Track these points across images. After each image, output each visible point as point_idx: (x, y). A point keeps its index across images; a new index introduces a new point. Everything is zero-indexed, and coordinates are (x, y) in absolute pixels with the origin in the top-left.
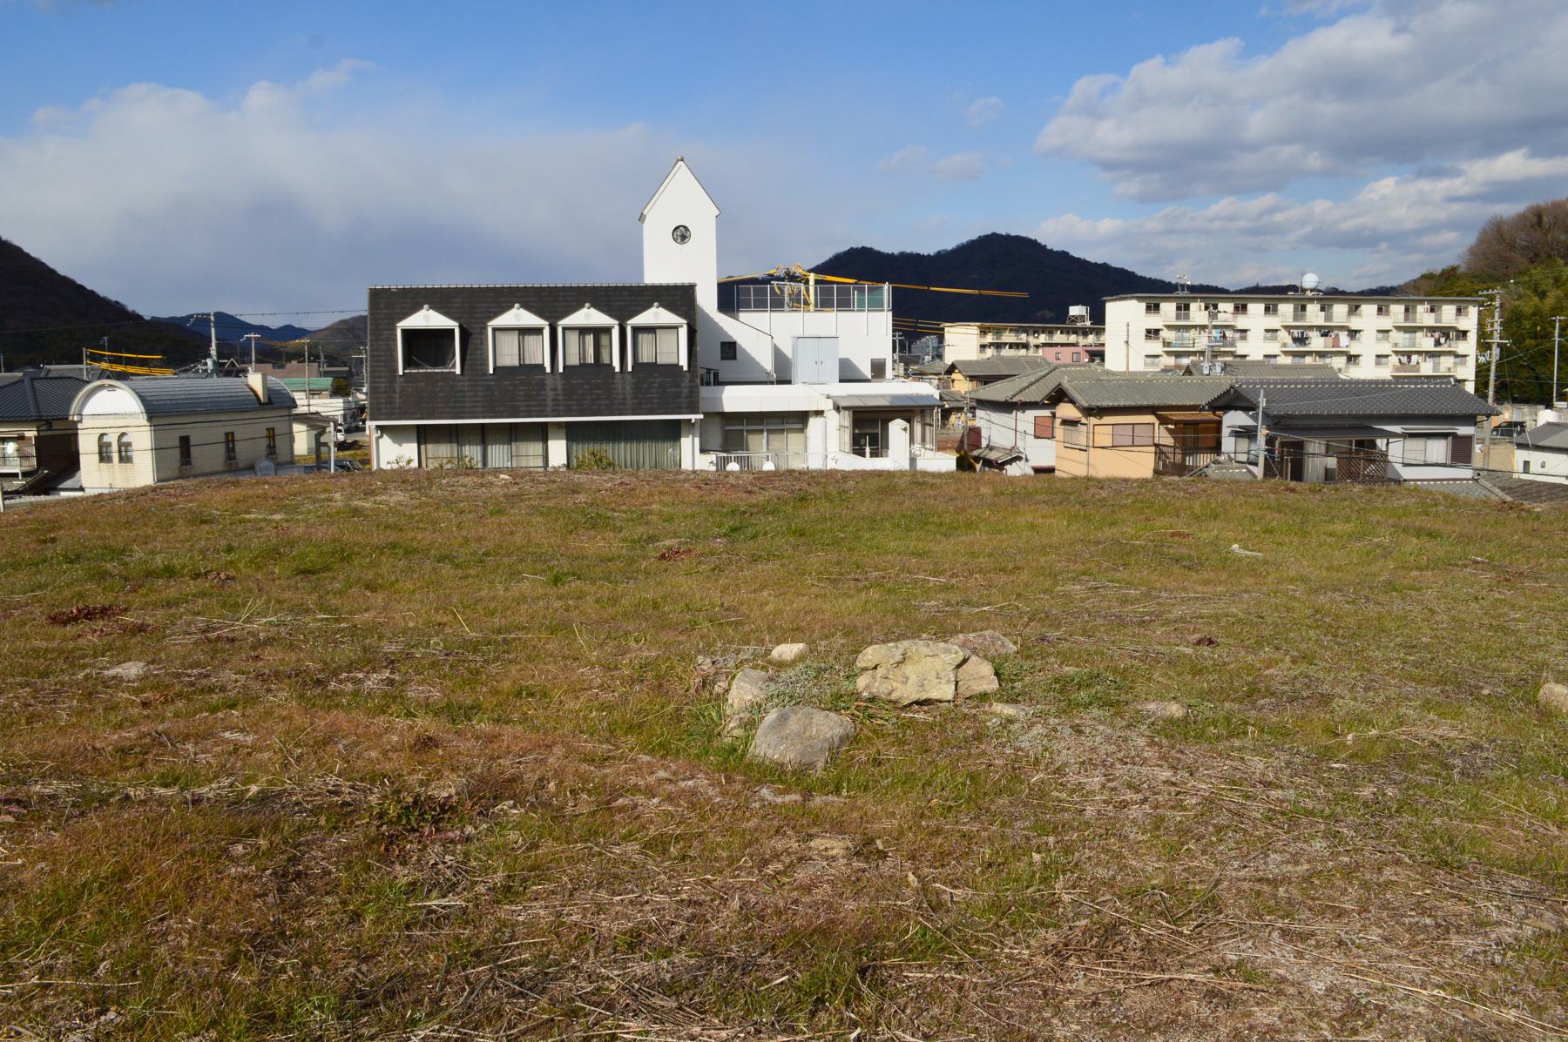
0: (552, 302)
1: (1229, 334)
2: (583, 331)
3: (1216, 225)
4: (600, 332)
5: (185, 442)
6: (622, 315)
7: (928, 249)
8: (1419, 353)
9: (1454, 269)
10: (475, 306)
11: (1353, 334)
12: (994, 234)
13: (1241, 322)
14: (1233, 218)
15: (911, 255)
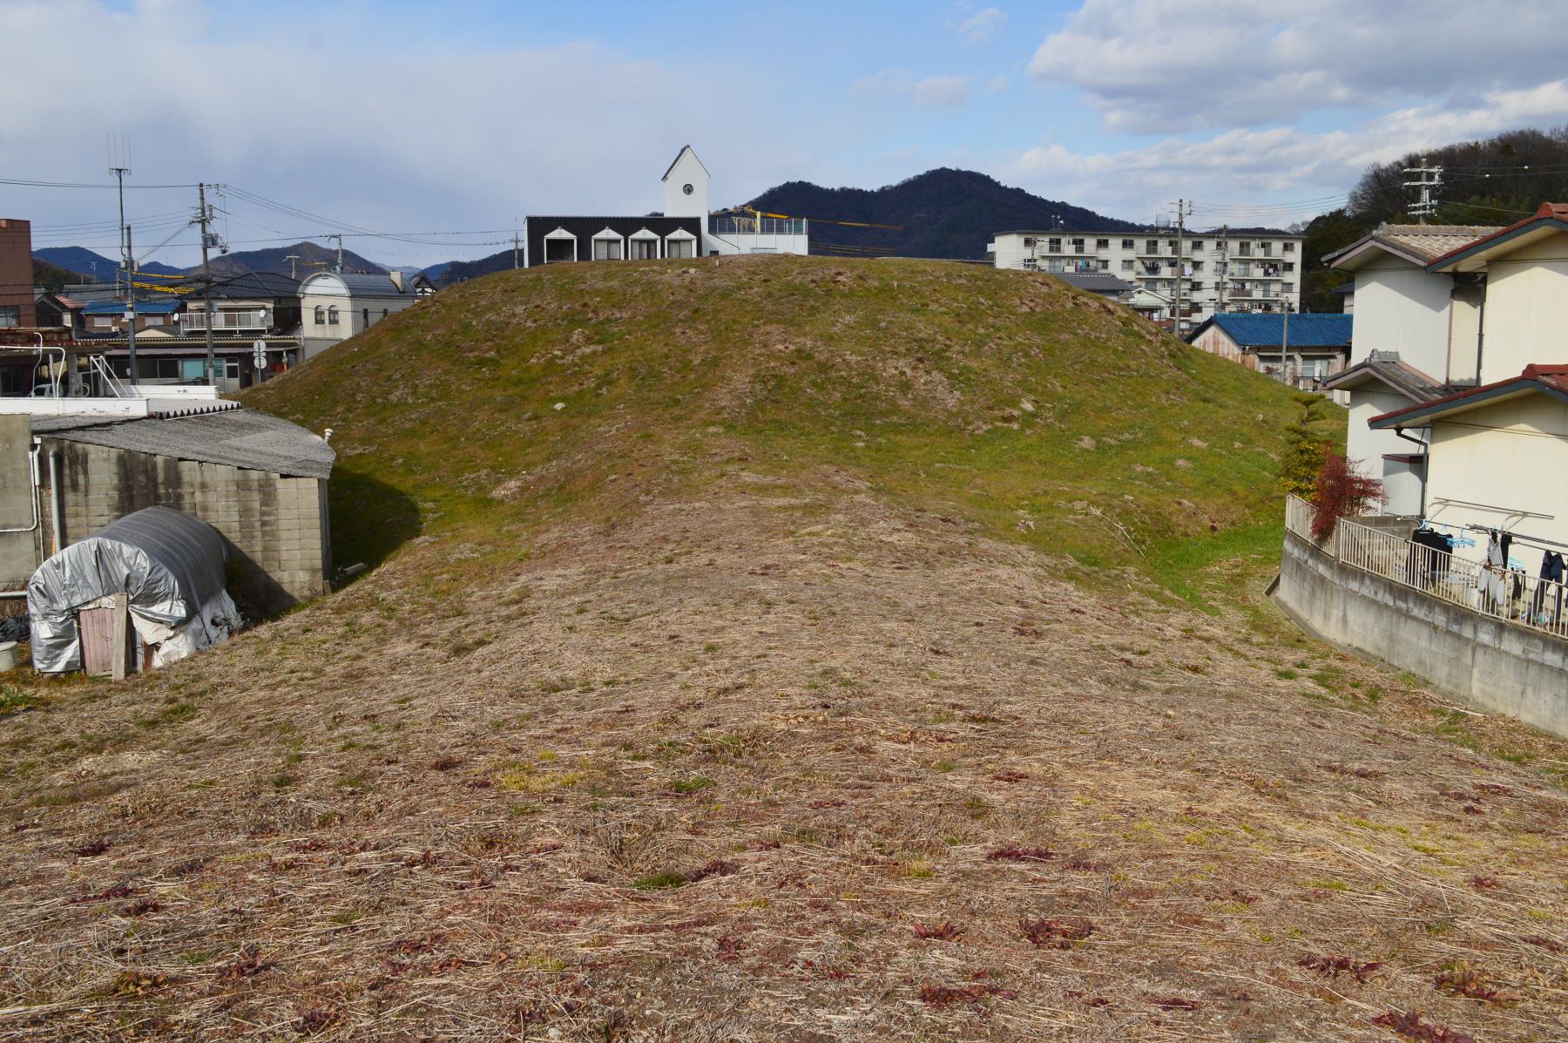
0: (625, 225)
1: (1093, 263)
2: (641, 242)
3: (1218, 160)
4: (651, 243)
5: (366, 312)
6: (663, 234)
7: (871, 184)
8: (1252, 281)
9: (1340, 212)
10: (585, 227)
11: (1197, 265)
12: (943, 169)
13: (1103, 254)
14: (1233, 151)
15: (852, 191)
